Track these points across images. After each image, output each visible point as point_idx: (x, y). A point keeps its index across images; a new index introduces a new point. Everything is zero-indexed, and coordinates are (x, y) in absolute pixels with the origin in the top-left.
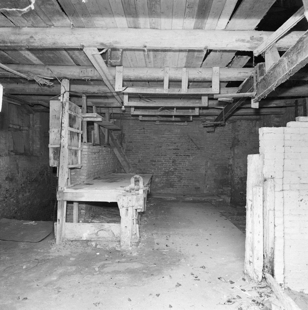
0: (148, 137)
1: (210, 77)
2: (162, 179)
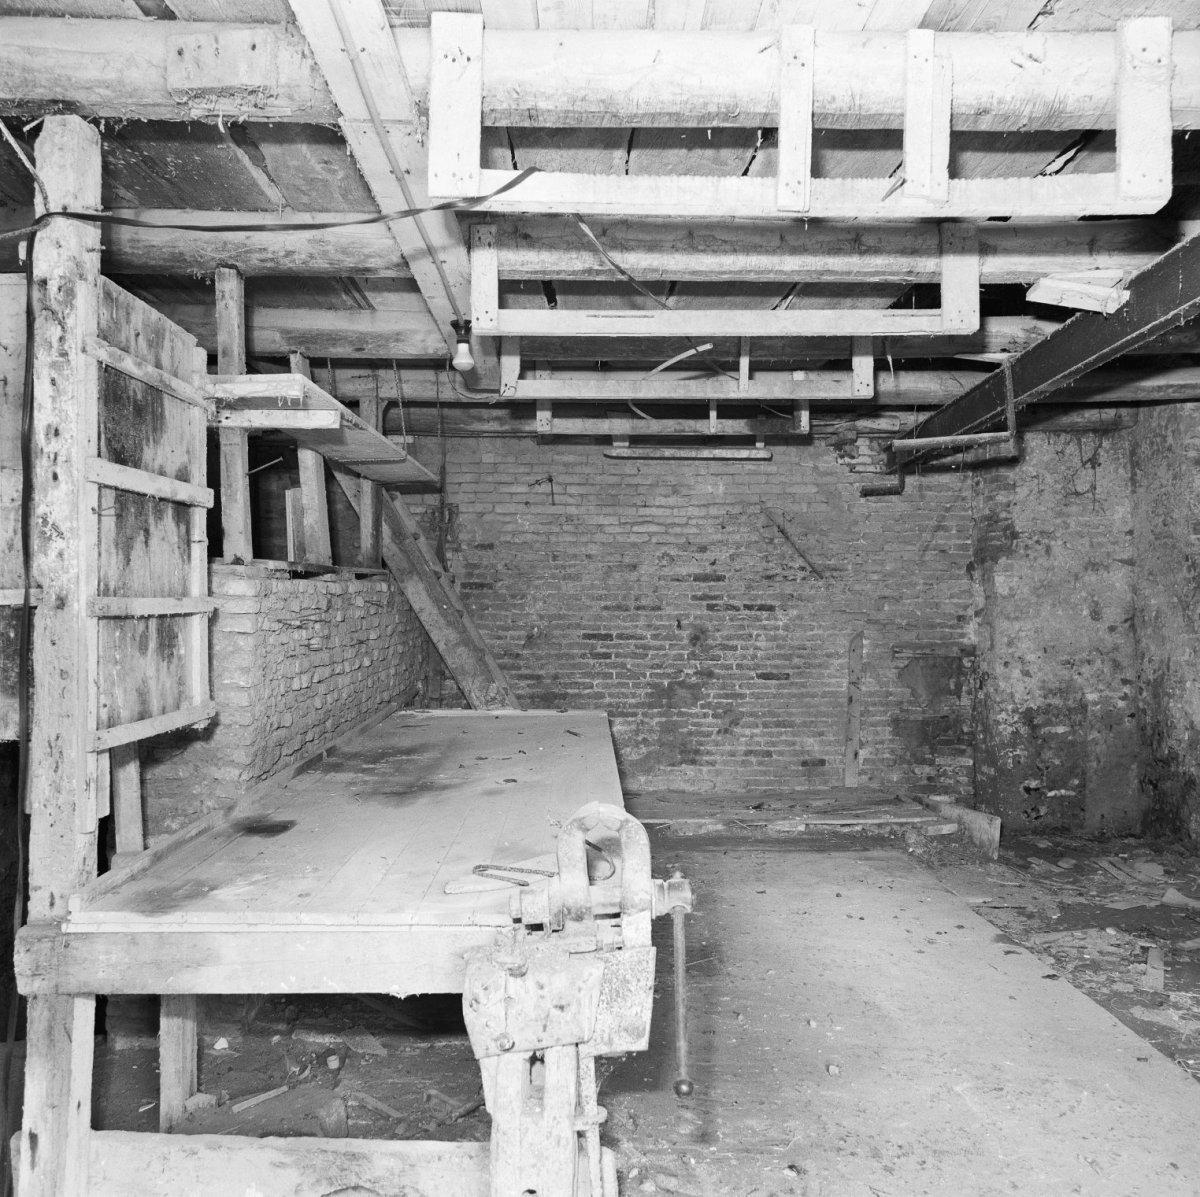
0: (569, 518)
1: (1102, 94)
2: (642, 722)
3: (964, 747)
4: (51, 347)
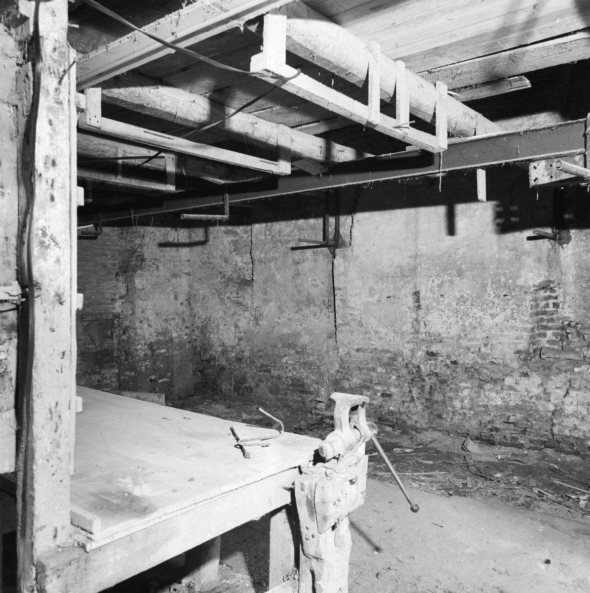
3: (114, 364)
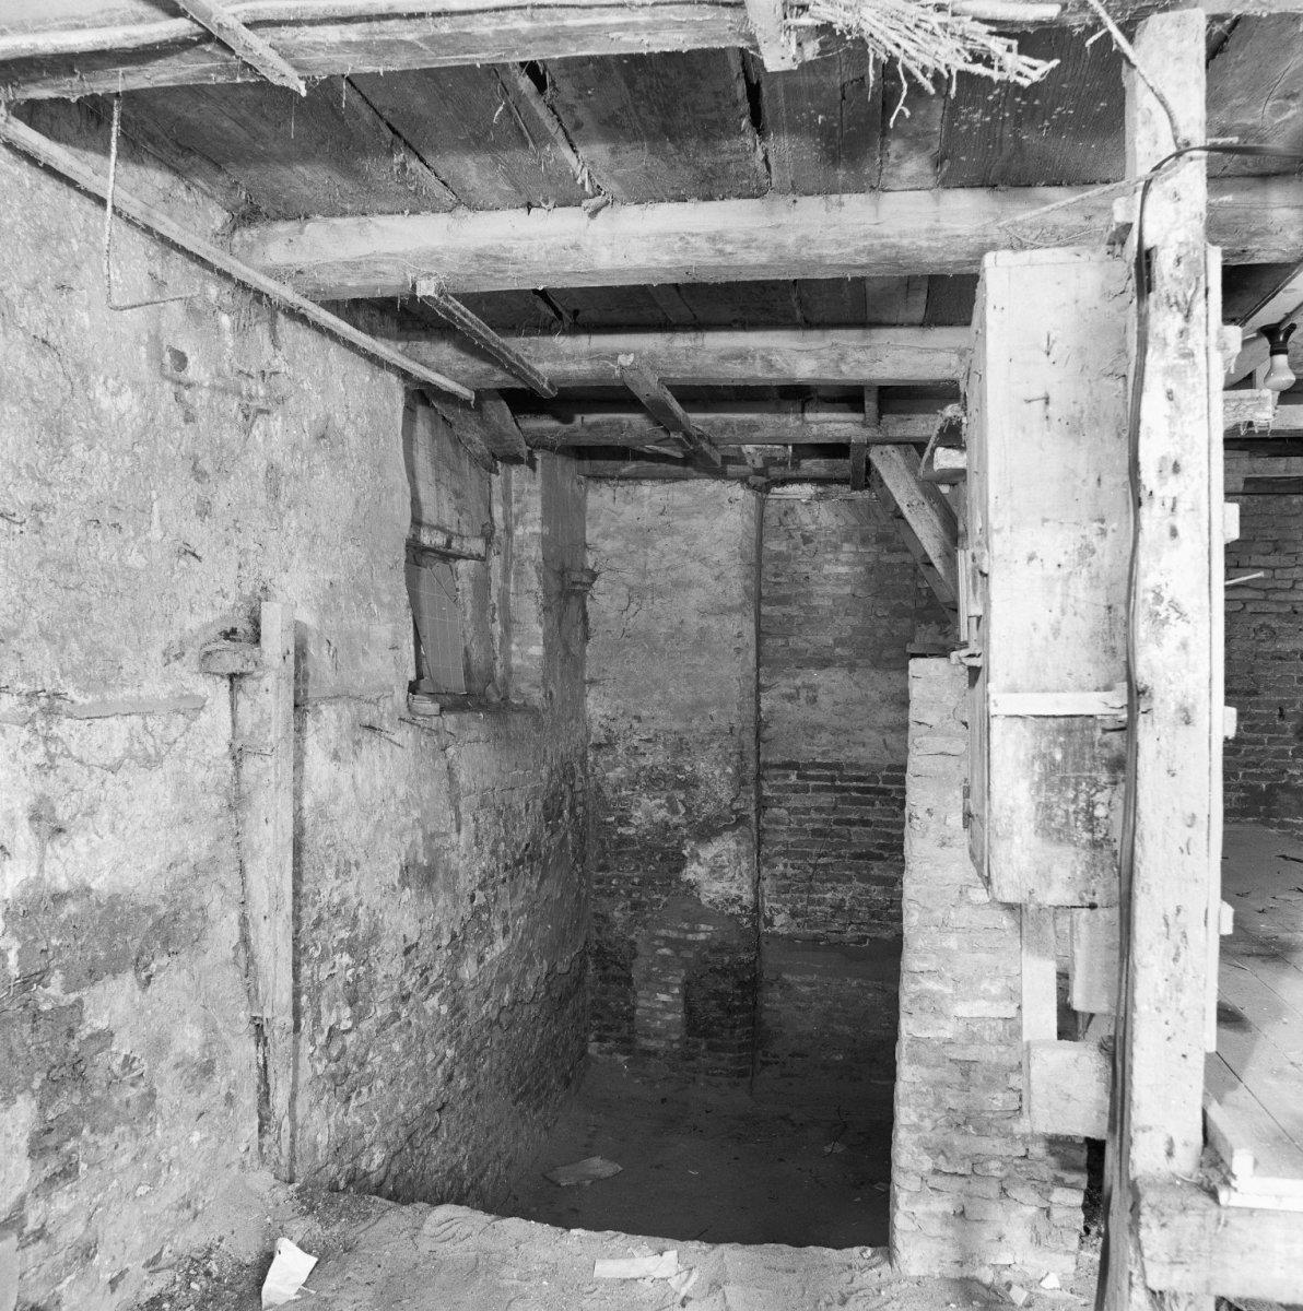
4: (1166, 345)
